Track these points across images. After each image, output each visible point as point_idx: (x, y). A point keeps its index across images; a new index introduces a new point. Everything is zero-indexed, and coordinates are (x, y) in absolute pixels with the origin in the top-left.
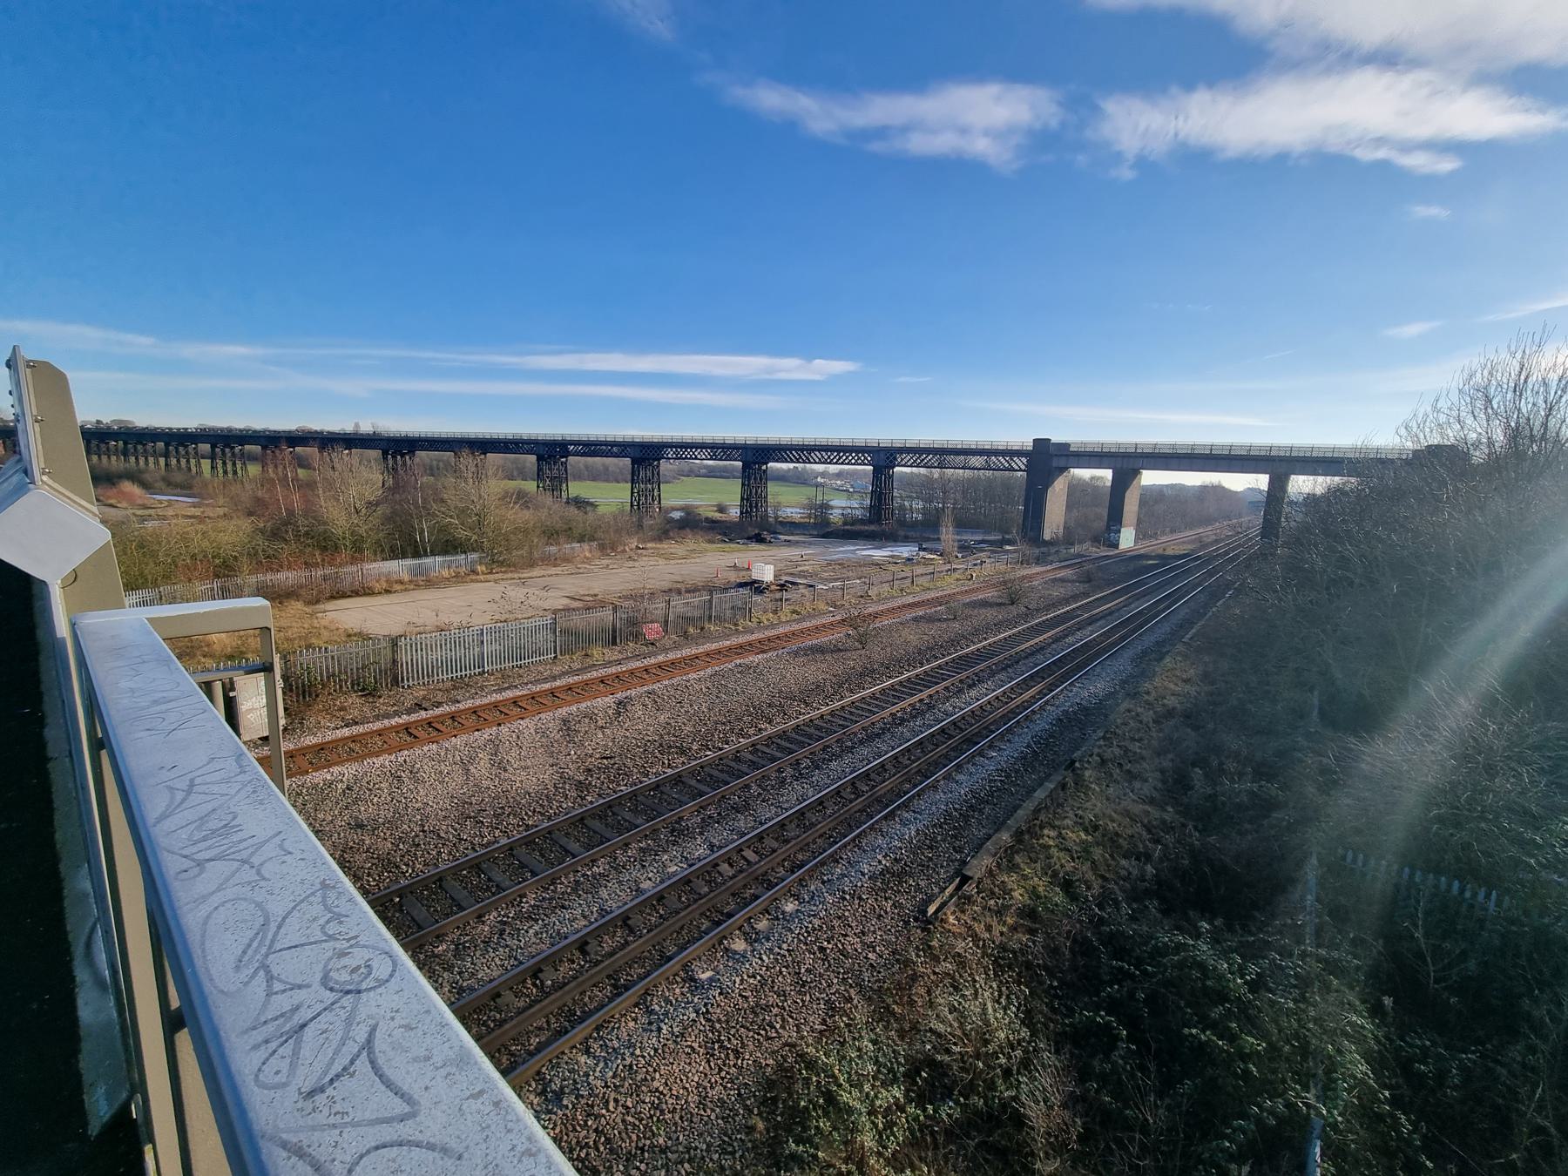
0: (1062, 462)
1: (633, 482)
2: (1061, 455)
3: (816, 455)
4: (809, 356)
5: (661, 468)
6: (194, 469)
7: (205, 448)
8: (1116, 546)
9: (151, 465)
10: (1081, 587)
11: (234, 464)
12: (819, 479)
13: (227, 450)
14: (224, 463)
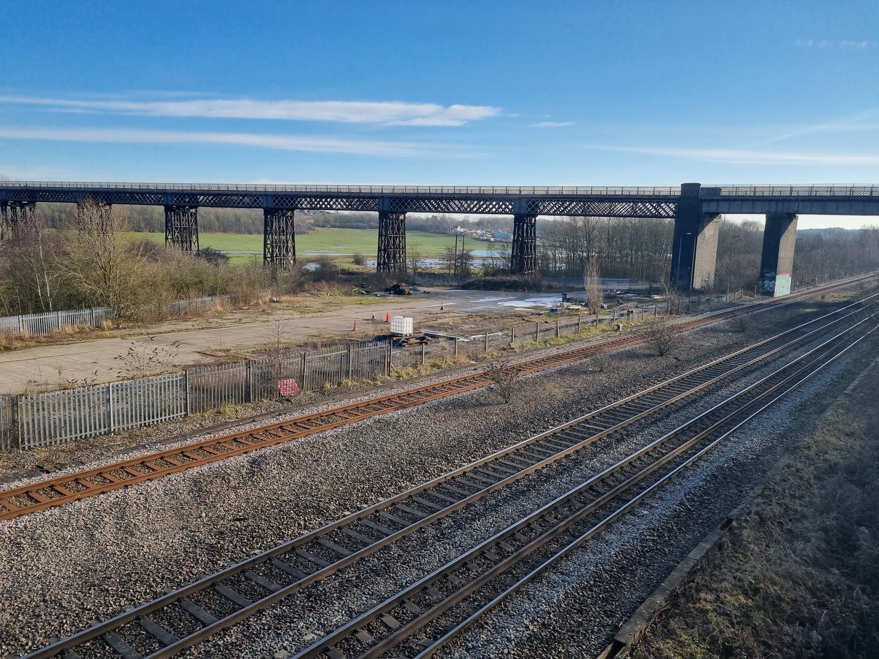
0: (712, 208)
2: (712, 200)
4: (446, 102)
8: (771, 293)
10: (735, 338)
12: (459, 229)
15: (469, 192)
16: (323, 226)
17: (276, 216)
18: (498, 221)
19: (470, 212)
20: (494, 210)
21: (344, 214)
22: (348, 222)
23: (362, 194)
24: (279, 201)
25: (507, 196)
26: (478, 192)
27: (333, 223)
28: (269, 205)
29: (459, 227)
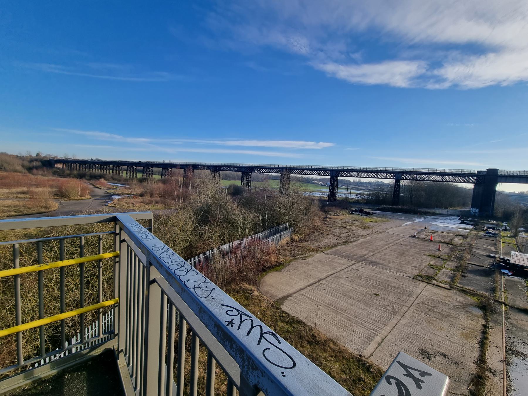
1: (162, 175)
3: (352, 174)
4: (318, 142)
7: (125, 167)
9: (108, 173)
11: (133, 173)
12: (314, 181)
13: (132, 168)
14: (130, 173)
19: (273, 173)
20: (315, 174)
21: (362, 181)
28: (244, 171)
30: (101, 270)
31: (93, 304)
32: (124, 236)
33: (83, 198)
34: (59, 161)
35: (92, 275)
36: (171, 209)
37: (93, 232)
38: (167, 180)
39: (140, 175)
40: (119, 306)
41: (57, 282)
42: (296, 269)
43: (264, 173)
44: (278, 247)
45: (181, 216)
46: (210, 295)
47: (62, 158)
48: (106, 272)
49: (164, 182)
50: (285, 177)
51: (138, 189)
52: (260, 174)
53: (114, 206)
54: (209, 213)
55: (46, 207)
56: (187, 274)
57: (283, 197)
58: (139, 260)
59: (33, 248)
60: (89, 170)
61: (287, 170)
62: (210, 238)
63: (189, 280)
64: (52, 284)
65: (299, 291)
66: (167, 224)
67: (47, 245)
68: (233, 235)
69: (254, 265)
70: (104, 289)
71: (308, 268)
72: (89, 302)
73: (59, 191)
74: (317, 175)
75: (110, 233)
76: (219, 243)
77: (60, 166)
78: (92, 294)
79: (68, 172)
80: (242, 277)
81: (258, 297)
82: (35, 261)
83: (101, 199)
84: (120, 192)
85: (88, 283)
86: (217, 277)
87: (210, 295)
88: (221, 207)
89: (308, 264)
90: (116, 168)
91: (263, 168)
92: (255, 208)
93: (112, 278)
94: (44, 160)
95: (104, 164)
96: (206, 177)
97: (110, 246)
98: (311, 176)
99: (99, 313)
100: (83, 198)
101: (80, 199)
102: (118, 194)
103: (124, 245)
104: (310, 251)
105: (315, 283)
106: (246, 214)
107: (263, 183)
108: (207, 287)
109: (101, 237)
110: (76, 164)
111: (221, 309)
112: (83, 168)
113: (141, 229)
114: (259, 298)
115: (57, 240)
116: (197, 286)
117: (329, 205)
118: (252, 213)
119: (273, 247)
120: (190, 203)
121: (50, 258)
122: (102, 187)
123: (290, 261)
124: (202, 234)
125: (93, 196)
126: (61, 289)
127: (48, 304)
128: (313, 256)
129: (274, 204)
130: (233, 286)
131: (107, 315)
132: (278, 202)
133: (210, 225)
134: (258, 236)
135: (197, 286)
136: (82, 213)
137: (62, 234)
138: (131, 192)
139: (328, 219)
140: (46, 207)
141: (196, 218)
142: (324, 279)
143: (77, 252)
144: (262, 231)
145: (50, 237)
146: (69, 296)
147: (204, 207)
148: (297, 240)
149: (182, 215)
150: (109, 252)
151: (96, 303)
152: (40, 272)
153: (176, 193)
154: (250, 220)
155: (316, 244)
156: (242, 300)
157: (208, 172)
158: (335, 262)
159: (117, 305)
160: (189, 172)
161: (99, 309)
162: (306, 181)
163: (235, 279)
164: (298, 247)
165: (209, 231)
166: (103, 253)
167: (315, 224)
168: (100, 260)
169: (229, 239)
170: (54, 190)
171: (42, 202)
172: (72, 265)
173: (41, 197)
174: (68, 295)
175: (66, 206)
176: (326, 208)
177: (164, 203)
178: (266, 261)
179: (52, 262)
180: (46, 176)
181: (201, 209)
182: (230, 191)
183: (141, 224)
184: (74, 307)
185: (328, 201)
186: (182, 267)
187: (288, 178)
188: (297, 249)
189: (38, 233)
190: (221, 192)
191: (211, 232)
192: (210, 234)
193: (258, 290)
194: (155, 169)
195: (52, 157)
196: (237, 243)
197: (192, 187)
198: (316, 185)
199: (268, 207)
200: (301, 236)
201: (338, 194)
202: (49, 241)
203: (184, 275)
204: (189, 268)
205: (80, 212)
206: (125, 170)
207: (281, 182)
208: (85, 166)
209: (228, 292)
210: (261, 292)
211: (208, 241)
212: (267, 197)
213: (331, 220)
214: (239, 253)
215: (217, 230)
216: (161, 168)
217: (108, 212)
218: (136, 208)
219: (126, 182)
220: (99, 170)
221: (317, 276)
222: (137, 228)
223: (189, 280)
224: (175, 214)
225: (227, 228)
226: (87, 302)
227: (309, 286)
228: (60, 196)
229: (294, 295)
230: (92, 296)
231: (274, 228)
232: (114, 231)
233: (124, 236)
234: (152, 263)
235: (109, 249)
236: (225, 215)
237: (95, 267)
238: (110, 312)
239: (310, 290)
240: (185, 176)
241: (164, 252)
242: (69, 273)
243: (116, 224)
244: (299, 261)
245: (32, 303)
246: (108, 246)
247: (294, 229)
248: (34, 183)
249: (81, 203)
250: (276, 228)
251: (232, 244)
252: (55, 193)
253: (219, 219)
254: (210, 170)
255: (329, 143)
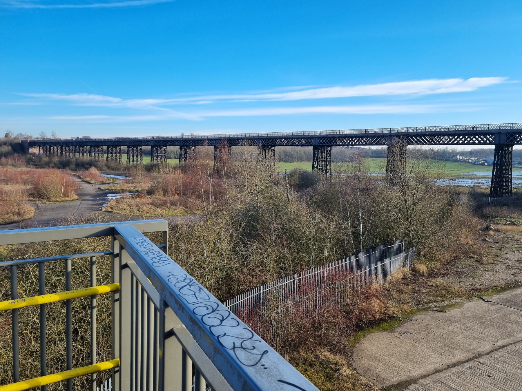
4: (466, 77)
5: (332, 151)
6: (118, 160)
7: (124, 148)
9: (100, 158)
11: (137, 156)
12: (458, 157)
13: (135, 149)
14: (133, 156)
15: (347, 133)
16: (365, 157)
17: (320, 150)
18: (484, 151)
20: (461, 142)
22: (380, 154)
23: (478, 132)
24: (323, 141)
25: (425, 133)
26: (352, 133)
27: (371, 155)
28: (317, 144)
29: (458, 155)
30: (95, 311)
31: (83, 366)
32: (127, 259)
33: (67, 199)
34: (34, 144)
35: (81, 320)
36: (196, 214)
37: (81, 251)
38: (189, 167)
39: (147, 160)
40: (120, 371)
41: (35, 328)
42: (424, 329)
43: (355, 146)
44: (387, 286)
45: (212, 226)
46: (259, 361)
47: (38, 138)
48: (101, 315)
49: (184, 169)
50: (397, 151)
51: (145, 183)
52: (348, 148)
53: (110, 210)
54: (258, 221)
55: (19, 214)
56: (222, 323)
57: (393, 189)
58: (149, 299)
59: (4, 275)
60: (75, 156)
61: (399, 138)
62: (261, 265)
63: (225, 334)
64: (28, 331)
65: (433, 374)
66: (190, 239)
67: (21, 271)
68: (301, 261)
69: (340, 319)
70: (98, 344)
71: (451, 328)
72: (77, 364)
73: (35, 188)
74: (465, 144)
75: (106, 254)
76: (275, 275)
77: (35, 150)
78: (81, 350)
79: (46, 159)
80: (318, 337)
81: (349, 378)
82: (6, 296)
83: (91, 200)
84: (119, 189)
85: (76, 332)
86: (274, 335)
87: (259, 361)
88: (277, 211)
89: (450, 321)
90: (112, 149)
91: (352, 137)
92: (339, 211)
93: (109, 327)
94: (14, 142)
95: (96, 144)
96: (251, 158)
97: (106, 274)
98: (450, 148)
99: (93, 381)
100: (67, 199)
101: (63, 201)
102: (115, 192)
103: (126, 273)
104: (454, 295)
105: (468, 361)
106: (322, 222)
107: (353, 164)
108: (254, 348)
109: (94, 259)
110: (57, 147)
111: (278, 387)
112: (66, 153)
113: (152, 248)
114: (352, 380)
115: (34, 263)
116: (238, 344)
117: (492, 204)
118: (333, 221)
119: (376, 284)
120: (225, 204)
121: (26, 291)
122: (93, 182)
123: (412, 313)
124: (246, 257)
125: (81, 195)
126: (40, 339)
127: (24, 362)
128: (460, 305)
129: (375, 203)
130: (302, 353)
131: (102, 385)
132: (384, 200)
133: (260, 242)
134: (346, 262)
135: (238, 344)
136: (67, 221)
137: (40, 255)
138: (135, 187)
139: (491, 232)
140: (19, 214)
141: (237, 230)
142: (487, 354)
143: (60, 284)
144: (354, 254)
145: (24, 258)
146: (50, 351)
147: (249, 211)
148: (425, 272)
149: (213, 225)
150: (105, 284)
151: (87, 365)
152: (14, 311)
153: (203, 187)
154: (330, 233)
155: (466, 283)
156: (320, 381)
157: (254, 150)
158: (511, 322)
159: (117, 370)
160: (223, 150)
161: (92, 374)
162: (442, 156)
163: (306, 340)
164: (427, 286)
165: (258, 252)
166: (97, 286)
167: (463, 241)
168: (93, 296)
169: (293, 266)
170: (29, 187)
171: (13, 206)
172: (54, 303)
173: (12, 199)
174: (49, 349)
175: (45, 211)
176: (487, 211)
177: (185, 204)
178: (363, 310)
179: (28, 297)
180: (17, 167)
181: (244, 214)
182: (293, 182)
183: (150, 239)
184: (57, 369)
185: (491, 195)
186: (215, 311)
187: (403, 154)
188: (425, 290)
189: (9, 253)
190: (277, 184)
191: (261, 254)
192: (261, 258)
193: (350, 365)
194: (170, 149)
195: (25, 138)
196: (306, 275)
197: (229, 176)
198: (462, 163)
199: (363, 208)
200: (432, 265)
201: (514, 181)
202: (24, 264)
203: (218, 325)
204: (225, 314)
205: (64, 220)
206: (125, 153)
207: (388, 161)
208: (69, 150)
209: (293, 362)
210: (355, 369)
211: (257, 270)
212: (362, 190)
213: (499, 233)
214: (311, 293)
215: (273, 250)
216: (178, 147)
217: (103, 221)
218: (143, 214)
219: (126, 172)
220: (89, 154)
221: (472, 347)
222: (144, 246)
223: (225, 334)
224: (202, 223)
225: (289, 248)
226: (75, 362)
227: (454, 365)
228: (36, 197)
229: (422, 381)
230: (81, 354)
231: (377, 248)
232: (112, 251)
233: (127, 259)
234: (169, 303)
235: (104, 278)
236: (286, 224)
237: (85, 308)
238: (106, 382)
239: (457, 374)
240: (217, 158)
241: (185, 286)
242: (50, 316)
243: (115, 239)
244: (430, 314)
245: (3, 358)
246: (104, 274)
247: (418, 252)
248: (4, 178)
249: (64, 207)
250: (380, 249)
251: (300, 276)
252: (30, 192)
253: (275, 231)
254: (258, 146)
255: (492, 78)
